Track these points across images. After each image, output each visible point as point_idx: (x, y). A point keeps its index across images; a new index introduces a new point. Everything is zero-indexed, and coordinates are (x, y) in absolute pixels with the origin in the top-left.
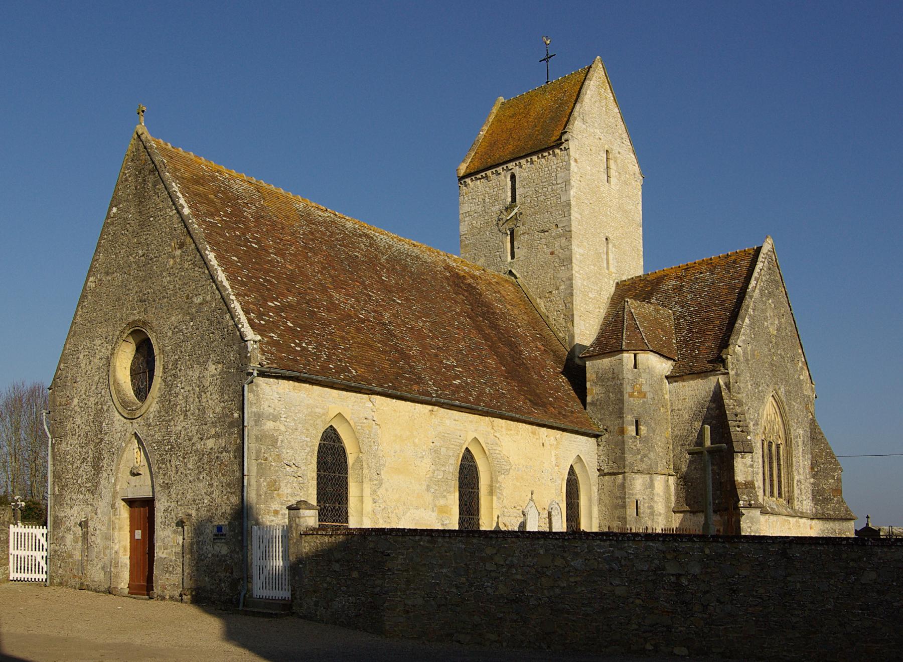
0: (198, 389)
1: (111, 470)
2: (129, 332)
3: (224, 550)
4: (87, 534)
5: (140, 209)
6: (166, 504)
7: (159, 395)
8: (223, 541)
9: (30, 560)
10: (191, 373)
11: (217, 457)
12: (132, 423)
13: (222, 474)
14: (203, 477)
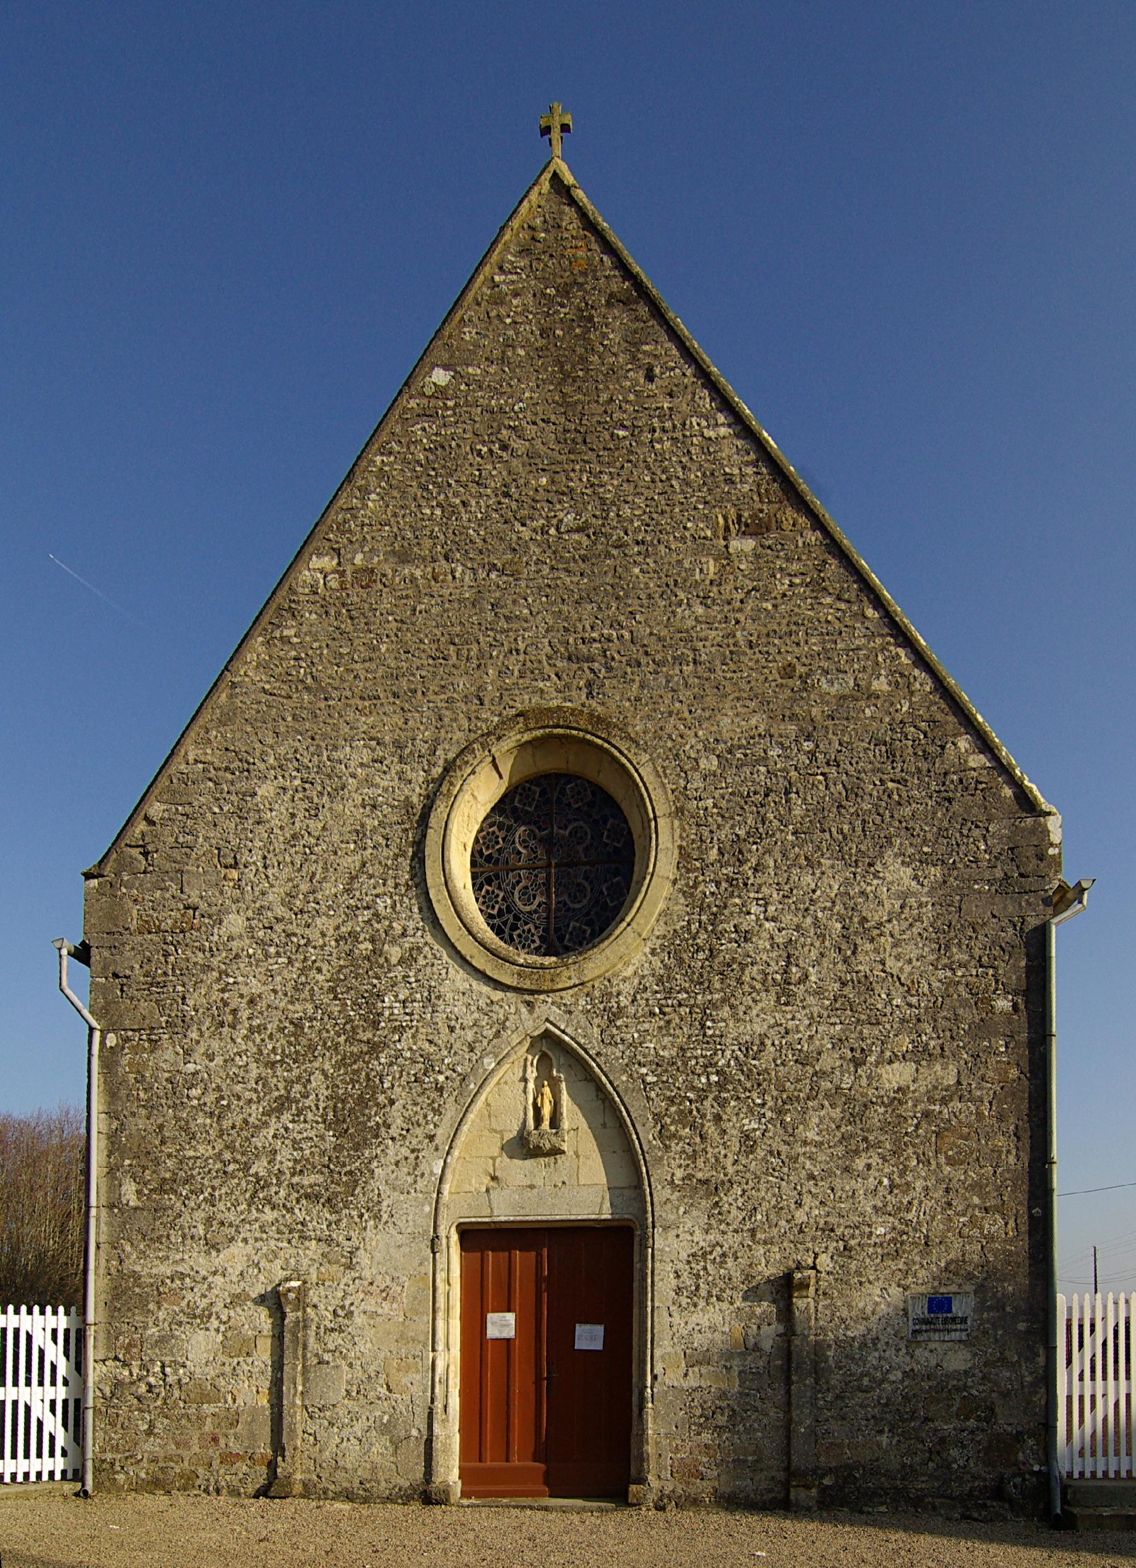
0: (839, 926)
1: (431, 1138)
2: (527, 737)
3: (958, 1361)
4: (305, 1327)
5: (564, 395)
6: (698, 1236)
7: (660, 930)
8: (955, 1336)
9: (1111, 1306)
10: (808, 880)
11: (927, 1114)
12: (529, 1004)
13: (948, 1158)
14: (869, 1167)
